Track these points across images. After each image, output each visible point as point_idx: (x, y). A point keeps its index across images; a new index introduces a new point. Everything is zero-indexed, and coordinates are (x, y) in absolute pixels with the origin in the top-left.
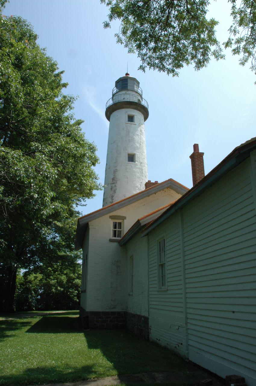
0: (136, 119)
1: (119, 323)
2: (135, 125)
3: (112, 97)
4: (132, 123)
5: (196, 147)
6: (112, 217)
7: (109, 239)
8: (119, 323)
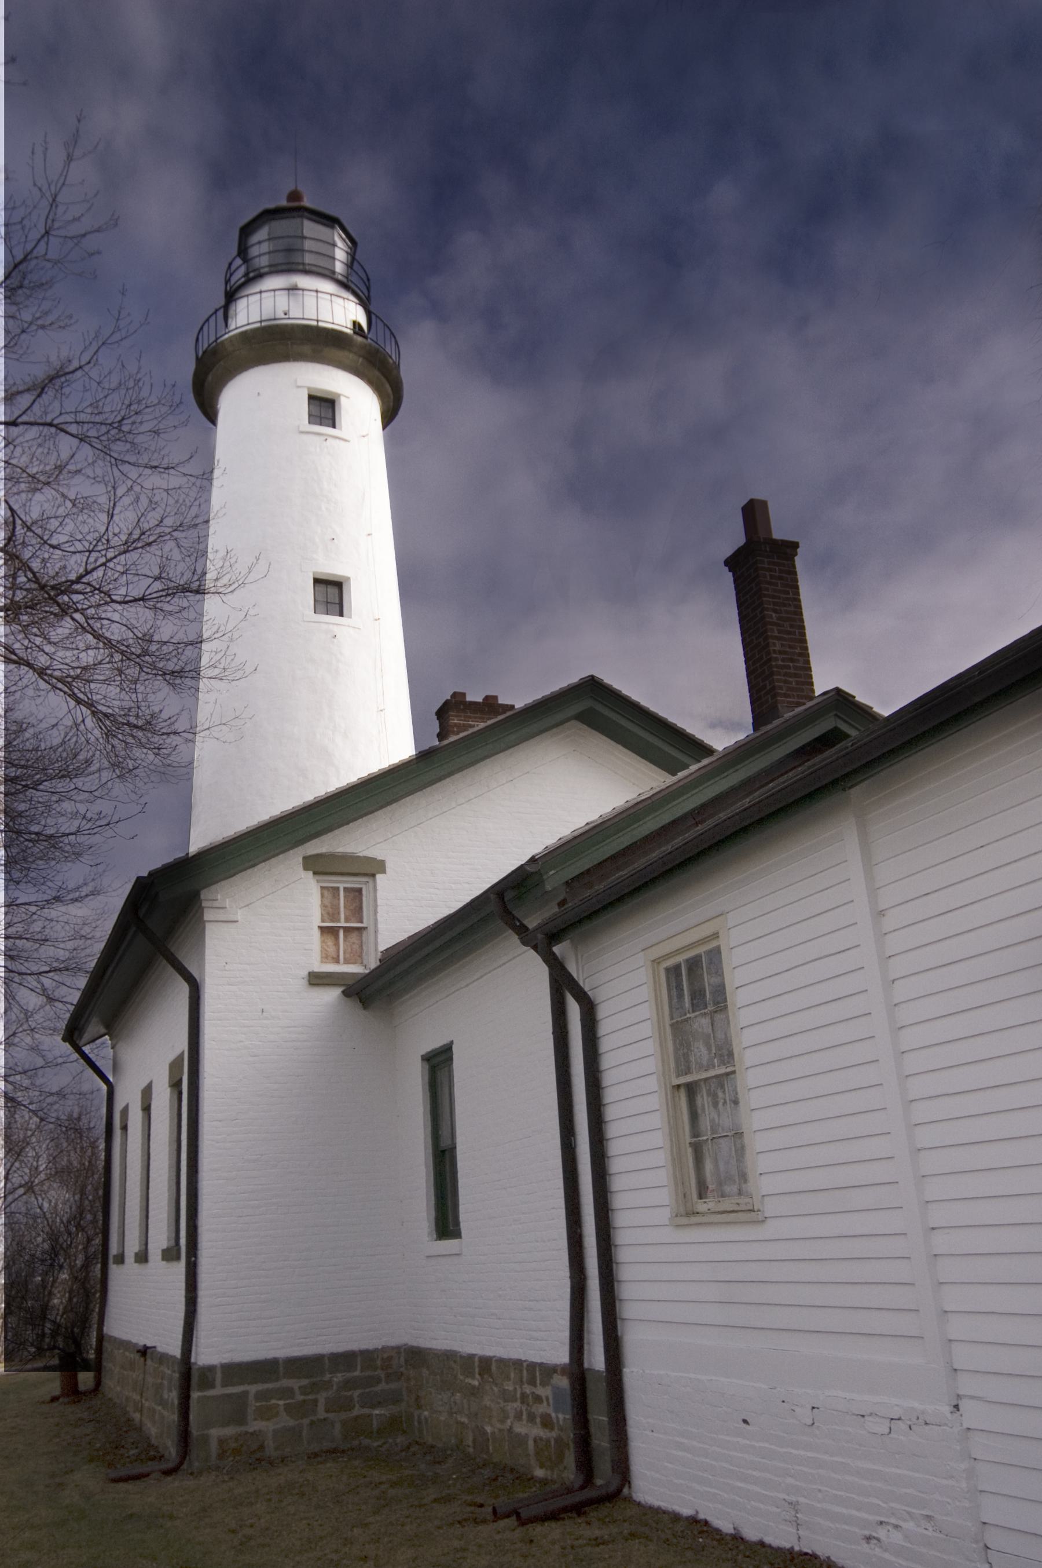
0: (346, 410)
1: (377, 1412)
2: (342, 443)
3: (222, 302)
4: (329, 430)
5: (754, 513)
6: (317, 865)
7: (305, 973)
8: (377, 1412)
